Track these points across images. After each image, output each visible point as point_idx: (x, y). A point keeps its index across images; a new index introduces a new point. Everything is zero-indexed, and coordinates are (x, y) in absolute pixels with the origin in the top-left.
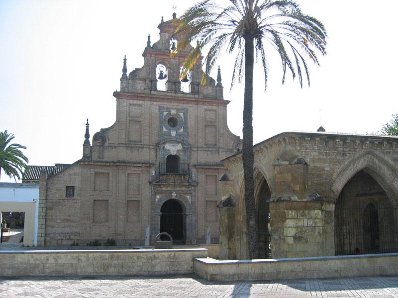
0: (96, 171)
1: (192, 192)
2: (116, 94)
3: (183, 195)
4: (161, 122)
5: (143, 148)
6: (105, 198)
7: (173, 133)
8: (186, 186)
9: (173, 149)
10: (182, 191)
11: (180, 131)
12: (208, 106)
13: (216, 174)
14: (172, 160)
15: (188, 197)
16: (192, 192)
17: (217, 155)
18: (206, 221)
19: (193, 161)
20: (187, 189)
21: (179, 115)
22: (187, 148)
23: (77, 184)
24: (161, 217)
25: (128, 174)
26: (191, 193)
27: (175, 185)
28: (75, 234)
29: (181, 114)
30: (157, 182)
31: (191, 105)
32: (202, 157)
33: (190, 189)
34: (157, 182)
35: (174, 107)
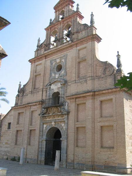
0: (19, 112)
1: (65, 120)
2: (99, 39)
3: (60, 123)
4: (51, 71)
5: (39, 91)
6: (84, 126)
7: (57, 76)
8: (59, 116)
9: (55, 88)
10: (58, 120)
11: (53, 76)
12: (80, 47)
13: (85, 102)
14: (56, 96)
15: (63, 125)
16: (65, 120)
17: (85, 84)
18: (102, 147)
19: (68, 94)
20: (61, 118)
21: (62, 61)
22: (65, 83)
23: (12, 121)
24: (46, 143)
25: (101, 102)
26: (65, 121)
27: (54, 116)
28: (8, 152)
29: (63, 60)
30: (42, 115)
31: (69, 51)
32: (73, 89)
33: (64, 117)
34: (42, 115)
35: (58, 57)
